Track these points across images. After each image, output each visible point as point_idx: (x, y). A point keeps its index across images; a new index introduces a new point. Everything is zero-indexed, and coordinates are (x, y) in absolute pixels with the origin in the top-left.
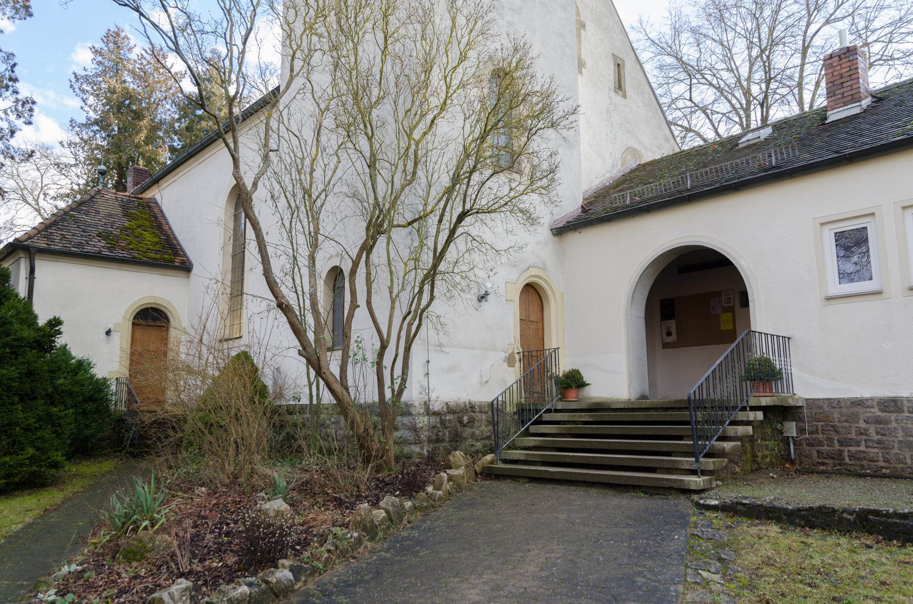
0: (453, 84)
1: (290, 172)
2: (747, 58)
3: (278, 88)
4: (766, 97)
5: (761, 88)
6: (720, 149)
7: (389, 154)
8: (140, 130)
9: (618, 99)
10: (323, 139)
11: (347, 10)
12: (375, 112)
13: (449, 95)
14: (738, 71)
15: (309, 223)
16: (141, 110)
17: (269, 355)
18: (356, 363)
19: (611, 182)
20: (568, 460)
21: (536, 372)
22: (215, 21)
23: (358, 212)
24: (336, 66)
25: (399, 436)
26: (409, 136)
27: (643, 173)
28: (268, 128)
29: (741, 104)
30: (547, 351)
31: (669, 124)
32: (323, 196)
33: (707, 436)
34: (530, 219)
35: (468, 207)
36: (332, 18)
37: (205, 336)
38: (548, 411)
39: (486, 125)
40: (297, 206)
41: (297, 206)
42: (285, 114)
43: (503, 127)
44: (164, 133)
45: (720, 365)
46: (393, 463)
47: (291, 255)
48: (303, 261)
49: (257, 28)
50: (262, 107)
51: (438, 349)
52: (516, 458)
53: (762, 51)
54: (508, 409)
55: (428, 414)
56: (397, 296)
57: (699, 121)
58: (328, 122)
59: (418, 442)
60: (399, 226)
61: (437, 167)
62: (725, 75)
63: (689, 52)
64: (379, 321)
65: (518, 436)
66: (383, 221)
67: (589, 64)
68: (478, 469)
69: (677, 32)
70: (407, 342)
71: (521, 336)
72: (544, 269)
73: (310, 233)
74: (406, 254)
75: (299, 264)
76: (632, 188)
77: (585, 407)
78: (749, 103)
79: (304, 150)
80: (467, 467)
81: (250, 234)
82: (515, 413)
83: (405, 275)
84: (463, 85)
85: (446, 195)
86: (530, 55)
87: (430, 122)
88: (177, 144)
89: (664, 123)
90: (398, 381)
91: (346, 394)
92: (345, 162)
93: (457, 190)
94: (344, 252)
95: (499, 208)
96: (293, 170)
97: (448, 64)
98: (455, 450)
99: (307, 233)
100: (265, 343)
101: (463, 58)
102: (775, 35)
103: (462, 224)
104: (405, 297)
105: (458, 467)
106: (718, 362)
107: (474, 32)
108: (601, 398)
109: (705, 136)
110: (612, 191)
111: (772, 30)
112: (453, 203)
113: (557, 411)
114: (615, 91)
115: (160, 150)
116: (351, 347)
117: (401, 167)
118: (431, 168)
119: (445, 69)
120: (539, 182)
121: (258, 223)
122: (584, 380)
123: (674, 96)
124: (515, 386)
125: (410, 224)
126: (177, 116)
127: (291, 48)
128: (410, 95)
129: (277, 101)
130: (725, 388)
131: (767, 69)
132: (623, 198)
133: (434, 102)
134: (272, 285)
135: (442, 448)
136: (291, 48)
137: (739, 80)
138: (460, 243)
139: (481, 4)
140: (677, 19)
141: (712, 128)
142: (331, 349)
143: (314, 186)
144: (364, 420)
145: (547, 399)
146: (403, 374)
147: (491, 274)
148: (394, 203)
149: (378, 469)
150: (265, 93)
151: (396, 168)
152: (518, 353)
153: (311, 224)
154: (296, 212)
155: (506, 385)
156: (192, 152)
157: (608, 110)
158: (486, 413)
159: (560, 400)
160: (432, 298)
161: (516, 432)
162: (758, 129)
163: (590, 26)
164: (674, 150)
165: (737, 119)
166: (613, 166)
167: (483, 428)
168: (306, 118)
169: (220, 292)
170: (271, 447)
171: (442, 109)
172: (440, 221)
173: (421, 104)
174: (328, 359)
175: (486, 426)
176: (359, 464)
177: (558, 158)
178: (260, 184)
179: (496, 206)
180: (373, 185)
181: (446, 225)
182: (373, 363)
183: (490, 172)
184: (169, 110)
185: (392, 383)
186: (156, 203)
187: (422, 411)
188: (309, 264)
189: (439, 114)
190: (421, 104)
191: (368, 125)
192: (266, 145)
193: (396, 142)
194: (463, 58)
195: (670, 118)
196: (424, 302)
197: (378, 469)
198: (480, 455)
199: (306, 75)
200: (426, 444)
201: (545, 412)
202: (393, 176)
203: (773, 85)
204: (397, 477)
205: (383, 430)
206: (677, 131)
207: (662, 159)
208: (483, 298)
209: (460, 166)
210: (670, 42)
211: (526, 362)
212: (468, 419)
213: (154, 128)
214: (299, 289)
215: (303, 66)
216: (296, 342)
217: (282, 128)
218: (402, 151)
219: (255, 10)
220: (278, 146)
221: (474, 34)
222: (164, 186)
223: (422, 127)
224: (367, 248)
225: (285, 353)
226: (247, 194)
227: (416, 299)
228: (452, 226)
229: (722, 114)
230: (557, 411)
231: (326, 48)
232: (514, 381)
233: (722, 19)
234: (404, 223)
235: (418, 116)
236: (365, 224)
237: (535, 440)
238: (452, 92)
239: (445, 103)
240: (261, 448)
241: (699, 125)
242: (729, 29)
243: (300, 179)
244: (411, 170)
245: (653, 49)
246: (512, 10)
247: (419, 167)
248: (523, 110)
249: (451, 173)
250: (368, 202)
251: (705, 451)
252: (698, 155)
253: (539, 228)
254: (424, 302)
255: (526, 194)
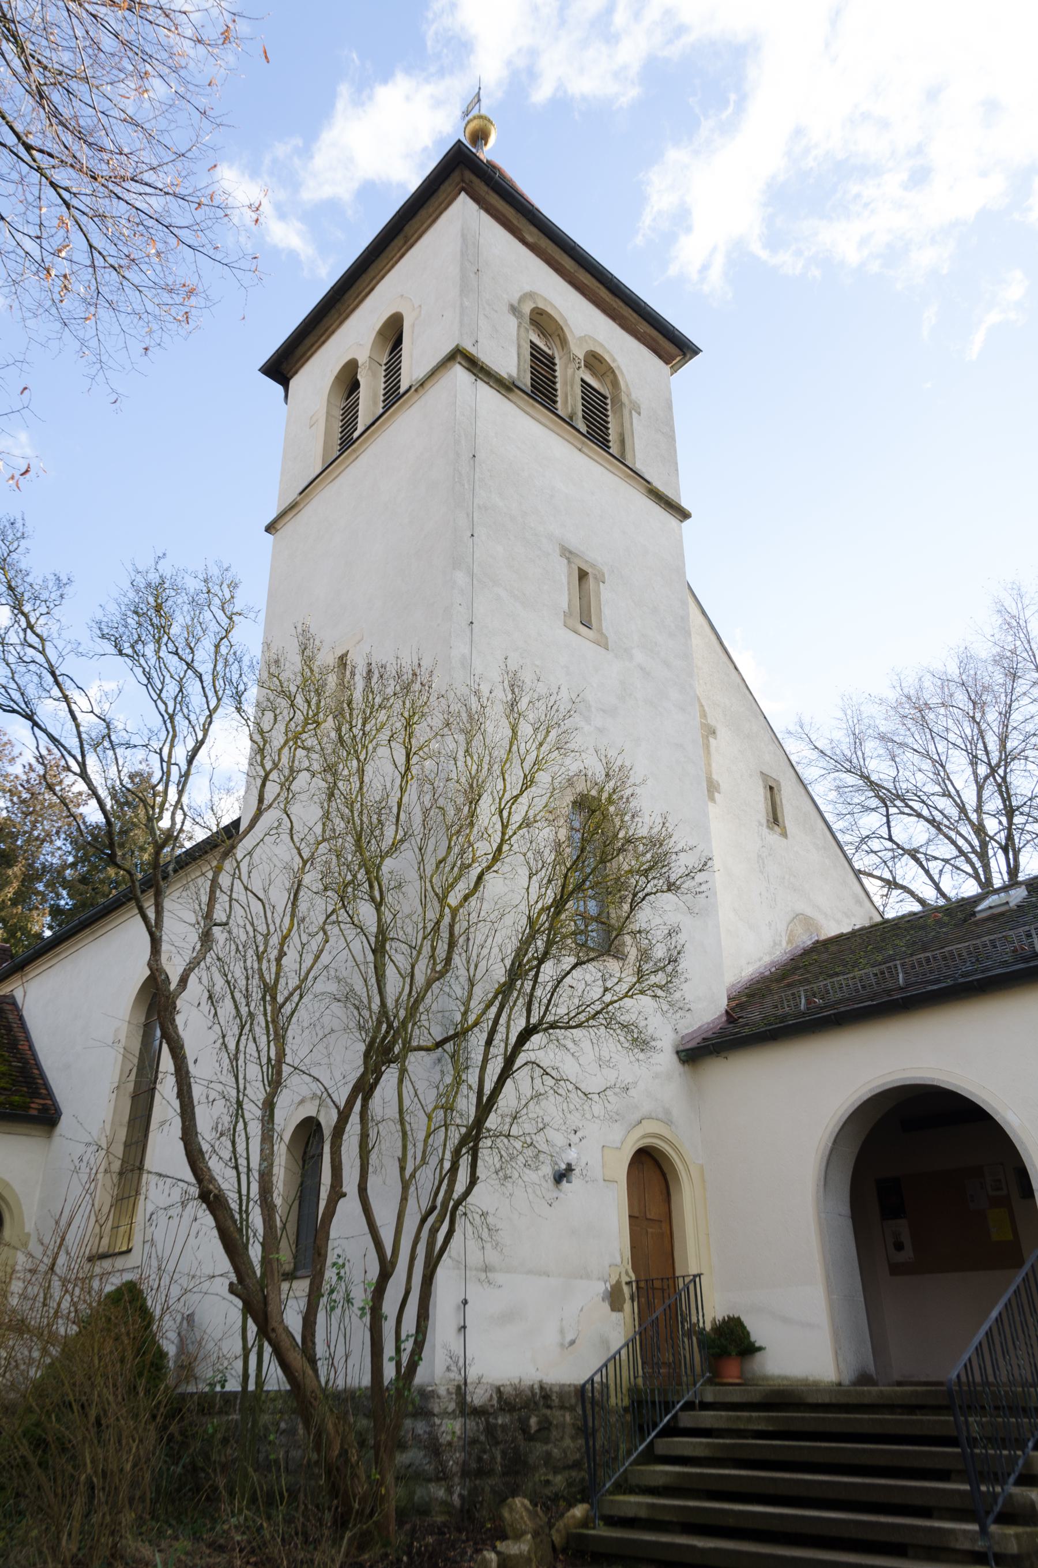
0: (512, 821)
1: (244, 956)
2: (972, 778)
3: (236, 823)
4: (1010, 837)
5: (1000, 823)
6: (946, 919)
7: (409, 930)
8: (8, 883)
9: (773, 838)
10: (303, 907)
11: (351, 714)
12: (388, 864)
13: (507, 837)
14: (959, 797)
15: (269, 1042)
16: (13, 850)
17: (175, 1291)
18: (333, 1309)
19: (773, 969)
20: (731, 1522)
21: (662, 1324)
22: (150, 730)
23: (352, 1025)
24: (331, 796)
25: (408, 1462)
26: (442, 899)
27: (825, 956)
28: (215, 884)
29: (972, 847)
30: (681, 1280)
31: (858, 873)
32: (296, 997)
33: (996, 1474)
34: (640, 1043)
35: (534, 1020)
36: (330, 723)
37: (62, 1259)
38: (689, 1406)
39: (564, 886)
40: (251, 1014)
41: (251, 1014)
42: (244, 866)
43: (592, 888)
44: (45, 886)
45: (999, 1319)
46: (393, 1527)
47: (234, 1101)
48: (253, 1111)
49: (212, 740)
50: (206, 852)
51: (483, 1276)
52: (630, 1513)
53: (993, 770)
54: (613, 1401)
55: (463, 1413)
56: (413, 1175)
57: (907, 871)
58: (311, 879)
59: (442, 1476)
60: (420, 1048)
61: (485, 952)
62: (943, 803)
63: (880, 770)
64: (379, 1222)
65: (636, 1462)
66: (394, 1042)
67: (724, 787)
68: (556, 1538)
69: (858, 741)
70: (426, 1267)
71: (633, 1248)
72: (668, 1123)
73: (269, 1059)
74: (430, 1098)
75: (247, 1115)
76: (807, 981)
77: (756, 1398)
78: (984, 845)
79: (270, 921)
80: (536, 1534)
81: (167, 1063)
82: (626, 1409)
83: (428, 1136)
84: (527, 823)
85: (500, 997)
86: (631, 781)
87: (475, 879)
88: (65, 902)
89: (852, 875)
90: (408, 1346)
91: (310, 1372)
92: (336, 941)
93: (518, 987)
94: (325, 1095)
95: (587, 1021)
96: (250, 952)
97: (505, 791)
98: (514, 1494)
99: (264, 1060)
100: (171, 1267)
101: (528, 782)
102: (1010, 745)
103: (525, 1048)
104: (426, 1179)
105: (518, 1537)
106: (994, 1314)
107: (545, 745)
108: (786, 1378)
109: (921, 895)
110: (774, 986)
111: (1003, 740)
112: (511, 1010)
113: (705, 1406)
114: (768, 827)
115: (35, 913)
116: (327, 1276)
117: (426, 950)
118: (474, 955)
119: (500, 799)
120: (652, 977)
121: (182, 1047)
122: (753, 1338)
123: (865, 833)
124: (624, 1352)
125: (439, 1044)
126: (71, 859)
127: (263, 766)
128: (445, 838)
129: (233, 847)
130: (1015, 1368)
131: (1005, 793)
132: (794, 999)
133: (484, 848)
134: (194, 1156)
135: (487, 1489)
136: (263, 766)
137: (962, 809)
138: (521, 1082)
139: (555, 708)
140: (856, 721)
141: (930, 883)
142: (290, 1276)
143: (282, 982)
144: (341, 1430)
145: (684, 1379)
146: (417, 1332)
147: (575, 1139)
148: (413, 1010)
149: (362, 1543)
150: (215, 830)
151: (419, 953)
152: (629, 1283)
153: (272, 1043)
154: (248, 1025)
155: (608, 1349)
156: (86, 919)
157: (759, 856)
158: (572, 1409)
159: (710, 1382)
160: (473, 1181)
161: (629, 1453)
162: (1005, 888)
163: (722, 732)
164: (871, 918)
165: (970, 870)
166: (775, 944)
167: (568, 1442)
168: (277, 871)
169: (102, 1169)
170: (158, 1491)
171: (495, 859)
172: (489, 1042)
173: (462, 852)
174: (284, 1296)
175: (573, 1438)
176: (326, 1532)
177: (682, 938)
178: (193, 979)
179: (582, 1017)
180: (378, 982)
181: (498, 1050)
182: (363, 1309)
183: (573, 960)
184: (59, 848)
185: (398, 1350)
186: (14, 1004)
187: (452, 1406)
188: (263, 1117)
189: (489, 868)
190: (462, 852)
191: (376, 884)
192: (208, 916)
193: (420, 910)
194: (528, 782)
195: (857, 866)
196: (460, 1188)
197: (362, 1543)
198: (562, 1504)
199: (282, 806)
200: (457, 1480)
201: (682, 1409)
202: (413, 967)
203: (1018, 819)
204: (399, 1560)
205: (376, 1447)
206: (873, 886)
207: (853, 933)
208: (562, 1176)
209: (526, 943)
210: (848, 753)
211: (643, 1300)
212: (539, 1423)
213: (30, 877)
214: (242, 1162)
215: (279, 795)
216: (224, 1264)
217: (238, 886)
218: (430, 926)
219: (210, 716)
220: (229, 917)
221: (545, 748)
222: (31, 975)
223: (462, 888)
224: (364, 1088)
225: (206, 1286)
226: (168, 998)
227: (446, 1181)
228: (509, 1050)
229: (943, 860)
230: (705, 1406)
231: (316, 767)
232: (622, 1342)
233: (923, 723)
234: (429, 1044)
235: (456, 869)
236: (362, 1047)
237: (666, 1473)
238: (511, 833)
239: (499, 849)
240: (138, 1494)
241: (908, 877)
242: (937, 739)
243: (260, 969)
244: (444, 955)
245: (823, 763)
246: (604, 711)
247: (457, 950)
248: (625, 862)
249: (508, 962)
250: (370, 1009)
251: (997, 1509)
252: (912, 928)
253: (655, 1055)
254: (460, 1188)
255: (631, 997)
